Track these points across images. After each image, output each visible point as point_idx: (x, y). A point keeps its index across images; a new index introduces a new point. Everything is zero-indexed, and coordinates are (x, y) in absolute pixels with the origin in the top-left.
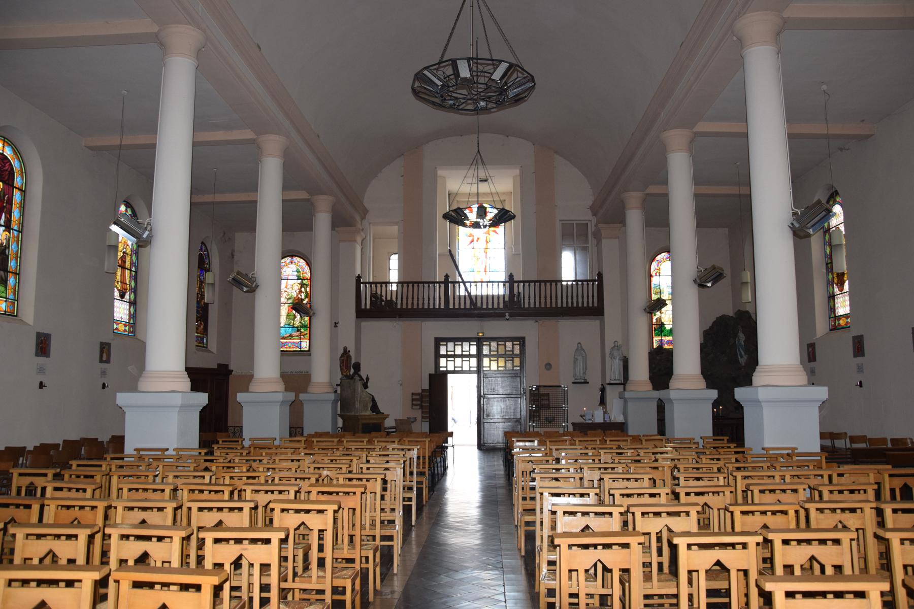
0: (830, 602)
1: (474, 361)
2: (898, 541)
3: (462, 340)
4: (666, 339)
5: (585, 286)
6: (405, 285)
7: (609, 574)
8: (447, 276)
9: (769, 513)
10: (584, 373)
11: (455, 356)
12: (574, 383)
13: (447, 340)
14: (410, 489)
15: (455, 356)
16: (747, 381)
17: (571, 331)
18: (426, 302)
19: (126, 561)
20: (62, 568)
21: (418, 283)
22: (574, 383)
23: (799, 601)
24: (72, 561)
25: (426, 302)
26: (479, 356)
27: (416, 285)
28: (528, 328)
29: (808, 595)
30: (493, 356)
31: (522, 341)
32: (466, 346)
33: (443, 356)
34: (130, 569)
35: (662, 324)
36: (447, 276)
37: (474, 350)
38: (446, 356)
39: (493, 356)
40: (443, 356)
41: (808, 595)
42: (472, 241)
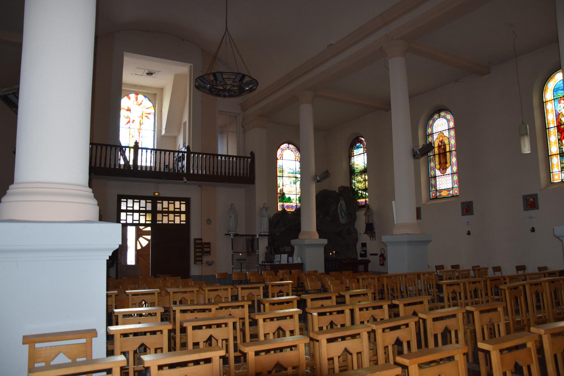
0: (191, 369)
1: (149, 218)
2: (381, 330)
3: (175, 199)
4: (286, 204)
5: (208, 160)
6: (158, 152)
7: (317, 343)
8: (136, 143)
9: (328, 314)
10: (236, 228)
11: (133, 211)
12: (226, 235)
13: (128, 197)
14: (235, 298)
15: (133, 211)
16: (297, 237)
17: (226, 196)
18: (215, 170)
19: (322, 327)
20: (338, 330)
21: (107, 146)
22: (226, 235)
23: (166, 371)
24: (343, 326)
25: (215, 170)
26: (154, 212)
27: (104, 148)
28: (192, 191)
29: (172, 366)
30: (143, 211)
31: (188, 202)
32: (177, 204)
33: (124, 211)
34: (326, 333)
35: (284, 194)
36: (136, 143)
37: (149, 207)
38: (126, 211)
39: (143, 211)
40: (124, 211)
41: (172, 366)
42: (129, 122)
